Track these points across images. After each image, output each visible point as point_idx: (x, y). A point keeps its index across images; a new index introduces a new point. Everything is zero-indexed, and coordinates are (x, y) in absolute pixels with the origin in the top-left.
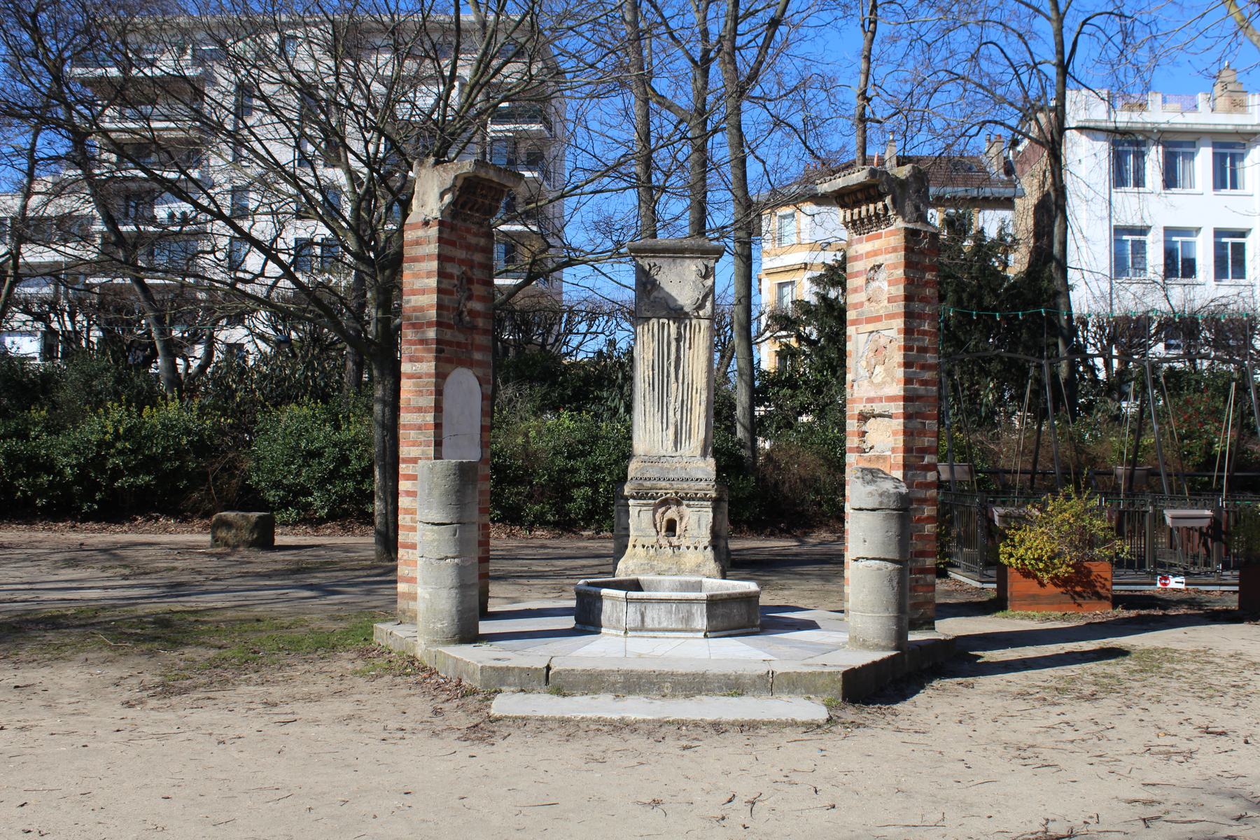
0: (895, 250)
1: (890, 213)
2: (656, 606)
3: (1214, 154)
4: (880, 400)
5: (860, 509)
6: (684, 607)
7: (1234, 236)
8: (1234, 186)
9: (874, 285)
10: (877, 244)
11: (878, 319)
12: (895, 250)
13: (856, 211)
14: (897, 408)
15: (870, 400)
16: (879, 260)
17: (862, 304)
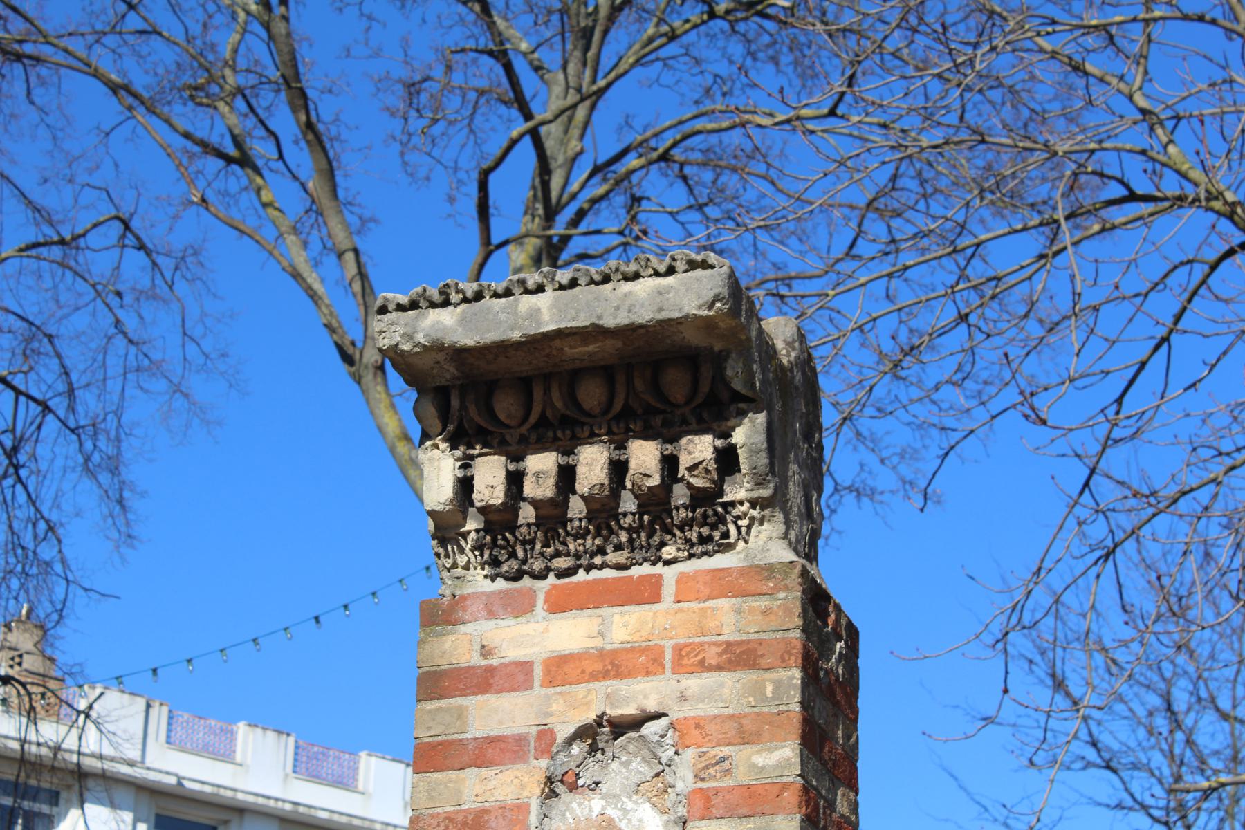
0: (740, 657)
1: (738, 491)
5: (1131, 320)
10: (623, 625)
12: (740, 657)
13: (541, 464)
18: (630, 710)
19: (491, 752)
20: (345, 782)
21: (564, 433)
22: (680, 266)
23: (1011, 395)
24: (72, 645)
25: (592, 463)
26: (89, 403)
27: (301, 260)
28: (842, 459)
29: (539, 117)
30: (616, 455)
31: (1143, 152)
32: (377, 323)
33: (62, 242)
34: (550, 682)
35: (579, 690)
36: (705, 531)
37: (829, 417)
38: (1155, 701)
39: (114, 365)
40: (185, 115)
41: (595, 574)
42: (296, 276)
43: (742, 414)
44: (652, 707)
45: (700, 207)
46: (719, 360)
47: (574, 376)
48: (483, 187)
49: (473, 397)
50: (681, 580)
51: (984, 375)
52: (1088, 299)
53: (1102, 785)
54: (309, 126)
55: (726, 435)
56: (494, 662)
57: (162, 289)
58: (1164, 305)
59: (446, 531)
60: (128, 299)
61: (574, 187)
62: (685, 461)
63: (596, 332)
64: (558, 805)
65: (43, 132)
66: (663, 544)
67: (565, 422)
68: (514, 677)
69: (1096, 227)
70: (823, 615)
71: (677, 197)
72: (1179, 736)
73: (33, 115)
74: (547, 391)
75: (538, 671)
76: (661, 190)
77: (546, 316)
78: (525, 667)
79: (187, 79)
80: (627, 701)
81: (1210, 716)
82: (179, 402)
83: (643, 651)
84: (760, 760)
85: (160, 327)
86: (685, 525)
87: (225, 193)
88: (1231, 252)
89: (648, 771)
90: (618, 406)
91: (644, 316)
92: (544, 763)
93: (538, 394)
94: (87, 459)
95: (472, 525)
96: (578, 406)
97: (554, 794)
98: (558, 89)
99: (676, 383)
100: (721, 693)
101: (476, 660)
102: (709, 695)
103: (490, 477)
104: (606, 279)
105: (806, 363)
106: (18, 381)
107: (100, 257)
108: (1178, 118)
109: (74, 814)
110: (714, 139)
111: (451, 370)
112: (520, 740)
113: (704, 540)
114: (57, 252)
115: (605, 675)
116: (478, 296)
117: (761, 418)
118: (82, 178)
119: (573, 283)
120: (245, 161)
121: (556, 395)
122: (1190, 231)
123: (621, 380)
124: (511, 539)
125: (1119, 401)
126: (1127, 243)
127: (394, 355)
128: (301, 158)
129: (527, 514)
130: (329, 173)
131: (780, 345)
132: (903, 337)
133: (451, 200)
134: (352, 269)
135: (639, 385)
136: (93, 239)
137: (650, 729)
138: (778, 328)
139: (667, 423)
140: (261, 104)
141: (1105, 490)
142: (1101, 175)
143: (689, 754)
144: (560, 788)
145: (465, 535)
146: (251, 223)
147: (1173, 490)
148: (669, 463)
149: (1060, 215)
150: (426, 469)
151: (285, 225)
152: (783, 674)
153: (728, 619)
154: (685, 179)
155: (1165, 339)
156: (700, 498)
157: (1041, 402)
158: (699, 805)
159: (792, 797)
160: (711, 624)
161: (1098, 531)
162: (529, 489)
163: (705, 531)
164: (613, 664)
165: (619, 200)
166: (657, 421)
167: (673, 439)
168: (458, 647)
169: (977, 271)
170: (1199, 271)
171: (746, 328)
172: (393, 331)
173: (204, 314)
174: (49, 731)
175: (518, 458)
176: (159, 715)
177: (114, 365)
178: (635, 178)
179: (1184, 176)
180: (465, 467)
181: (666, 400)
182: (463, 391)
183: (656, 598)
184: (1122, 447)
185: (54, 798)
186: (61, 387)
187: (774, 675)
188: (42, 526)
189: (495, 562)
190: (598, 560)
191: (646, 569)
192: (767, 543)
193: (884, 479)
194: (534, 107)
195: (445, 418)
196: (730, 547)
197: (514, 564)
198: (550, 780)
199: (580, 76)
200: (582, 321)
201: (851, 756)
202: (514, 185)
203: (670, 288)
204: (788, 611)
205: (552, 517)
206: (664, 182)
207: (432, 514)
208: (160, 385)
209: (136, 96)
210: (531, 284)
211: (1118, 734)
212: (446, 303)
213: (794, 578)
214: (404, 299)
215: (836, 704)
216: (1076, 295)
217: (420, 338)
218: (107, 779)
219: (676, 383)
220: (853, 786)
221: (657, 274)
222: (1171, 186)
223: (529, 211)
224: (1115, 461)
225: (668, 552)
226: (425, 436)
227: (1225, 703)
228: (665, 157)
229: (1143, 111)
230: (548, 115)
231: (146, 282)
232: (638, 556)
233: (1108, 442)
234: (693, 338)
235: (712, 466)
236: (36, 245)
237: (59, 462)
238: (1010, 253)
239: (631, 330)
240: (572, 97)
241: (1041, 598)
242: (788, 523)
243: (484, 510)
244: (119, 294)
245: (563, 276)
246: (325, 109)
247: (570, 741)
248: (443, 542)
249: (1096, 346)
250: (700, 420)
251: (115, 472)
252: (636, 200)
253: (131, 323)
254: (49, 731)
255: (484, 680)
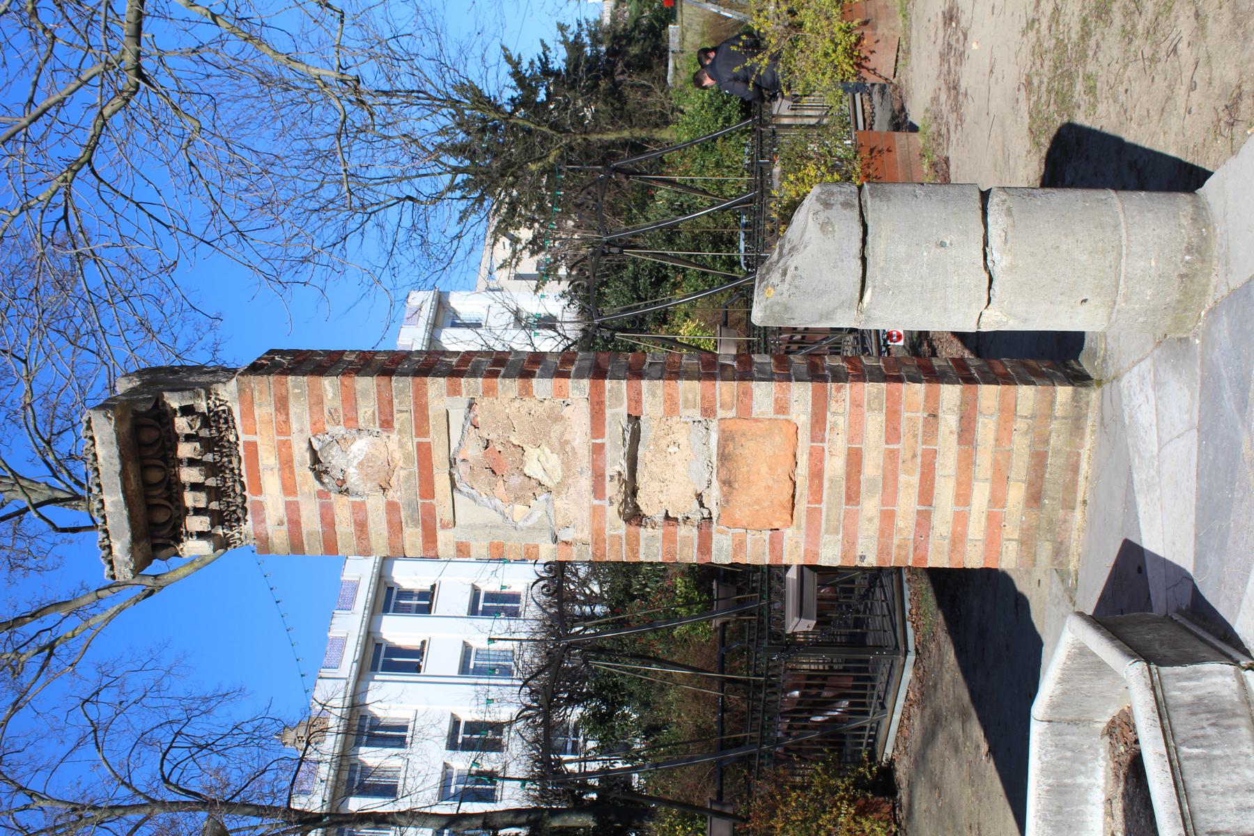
0: (282, 404)
1: (202, 406)
2: (1199, 800)
3: (367, 745)
4: (598, 450)
6: (1180, 721)
7: (457, 733)
8: (405, 728)
9: (354, 478)
10: (268, 459)
11: (424, 453)
12: (282, 404)
13: (190, 499)
14: (616, 389)
15: (598, 489)
16: (301, 455)
17: (392, 507)
18: (308, 455)
19: (328, 520)
20: (355, 587)
21: (174, 489)
22: (89, 433)
23: (164, 276)
24: (293, 715)
25: (189, 475)
26: (175, 713)
27: (101, 617)
28: (200, 357)
29: (27, 504)
30: (185, 464)
31: (43, 212)
32: (120, 578)
33: (95, 731)
34: (294, 493)
35: (298, 479)
36: (222, 421)
37: (177, 363)
38: (314, 216)
39: (158, 703)
40: (26, 679)
41: (243, 473)
42: (110, 618)
43: (164, 403)
44: (306, 445)
45: (74, 426)
46: (137, 415)
47: (146, 485)
48: (64, 530)
49: (156, 530)
50: (246, 432)
51: (159, 291)
52: (118, 240)
53: (353, 241)
54: (33, 616)
55: (175, 411)
56: (286, 519)
57: (118, 682)
58: (120, 204)
59: (223, 544)
60: (123, 698)
61: (63, 486)
62: (188, 431)
63: (124, 474)
64: (352, 488)
65: (39, 743)
66: (228, 441)
67: (169, 488)
68: (293, 511)
69: (81, 235)
70: (263, 366)
71: (69, 436)
72: (330, 206)
73: (30, 749)
74: (153, 497)
75: (290, 499)
76: (64, 445)
77: (115, 498)
78: (288, 504)
79: (9, 676)
80: (303, 457)
81: (321, 192)
82: (173, 671)
83: (280, 450)
84: (330, 395)
85: (136, 683)
86: (219, 430)
87: (69, 656)
88: (93, 171)
89: (336, 447)
90: (161, 463)
91: (115, 451)
92: (333, 495)
93: (155, 501)
94: (203, 713)
95: (220, 531)
96: (161, 482)
97: (347, 490)
98: (13, 495)
99: (149, 435)
100: (299, 414)
101: (285, 527)
102: (300, 418)
103: (196, 523)
104: (96, 469)
105: (140, 373)
106: (165, 747)
107: (101, 712)
108: (26, 195)
109: (370, 708)
110: (39, 419)
111: (143, 543)
112: (322, 506)
113: (226, 421)
114: (100, 734)
115: (291, 467)
116: (106, 531)
117: (166, 394)
118: (62, 724)
119: (99, 485)
120: (51, 646)
121: (155, 493)
122: (83, 191)
123: (147, 462)
124: (227, 512)
125: (168, 227)
126: (89, 221)
127: (137, 571)
128: (50, 619)
129: (214, 505)
130: (57, 605)
131: (130, 386)
132: (136, 328)
133: (71, 542)
134: (106, 592)
135: (150, 453)
136: (94, 717)
137: (316, 446)
138: (123, 386)
139: (169, 440)
140: (22, 640)
141: (212, 235)
142: (54, 232)
143: (328, 428)
144: (344, 487)
145: (225, 535)
146: (84, 643)
147: (210, 203)
148: (189, 438)
149: (74, 252)
150: (193, 554)
151: (83, 625)
152: (290, 384)
153: (264, 410)
154: (60, 433)
155: (137, 204)
156: (206, 422)
157: (167, 262)
158: (351, 423)
159: (347, 380)
160: (267, 418)
161: (232, 239)
162: (202, 505)
163: (222, 421)
164: (286, 464)
165: (70, 464)
166: (168, 444)
167: (177, 436)
168: (279, 536)
169: (105, 293)
170: (103, 187)
171: (121, 401)
172: (124, 572)
173: (131, 661)
174: (333, 722)
175: (187, 510)
176: (325, 672)
177: (158, 703)
178: (59, 457)
179: (55, 193)
180: (191, 535)
181: (157, 441)
182: (153, 537)
183: (254, 444)
184: (190, 226)
185: (363, 717)
186: (167, 727)
187: (291, 389)
188: (235, 732)
189: (238, 520)
190: (237, 472)
191: (241, 449)
192: (227, 392)
193: (209, 338)
194: (22, 506)
195: (168, 546)
196: (230, 409)
197: (239, 511)
198: (340, 492)
199: (6, 485)
200: (118, 481)
201: (329, 353)
202: (63, 516)
203: (101, 439)
204: (260, 382)
205: (216, 493)
206: (61, 443)
207: (215, 551)
208: (166, 681)
209: (18, 701)
210: (99, 506)
211: (330, 234)
212: (109, 547)
213: (245, 379)
214: (108, 567)
215: (304, 360)
216: (114, 245)
217: (127, 558)
218: (354, 695)
219: (149, 435)
220: (342, 353)
221: (94, 445)
222: (60, 199)
223: (75, 508)
224: (197, 230)
225: (232, 438)
226: (177, 555)
227: (316, 185)
228: (48, 443)
229: (21, 211)
230: (26, 499)
231: (116, 690)
232: (234, 452)
233: (188, 233)
234: (126, 427)
235: (190, 418)
236: (97, 743)
237: (205, 726)
238: (93, 276)
239: (123, 458)
240: (17, 488)
241: (265, 267)
242: (218, 382)
243: (213, 526)
244: (121, 703)
245: (95, 490)
246: (24, 608)
247: (322, 483)
248: (229, 545)
249: (141, 237)
250: (167, 424)
251: (210, 699)
252: (71, 456)
253: (136, 696)
254: (333, 722)
255: (294, 524)
